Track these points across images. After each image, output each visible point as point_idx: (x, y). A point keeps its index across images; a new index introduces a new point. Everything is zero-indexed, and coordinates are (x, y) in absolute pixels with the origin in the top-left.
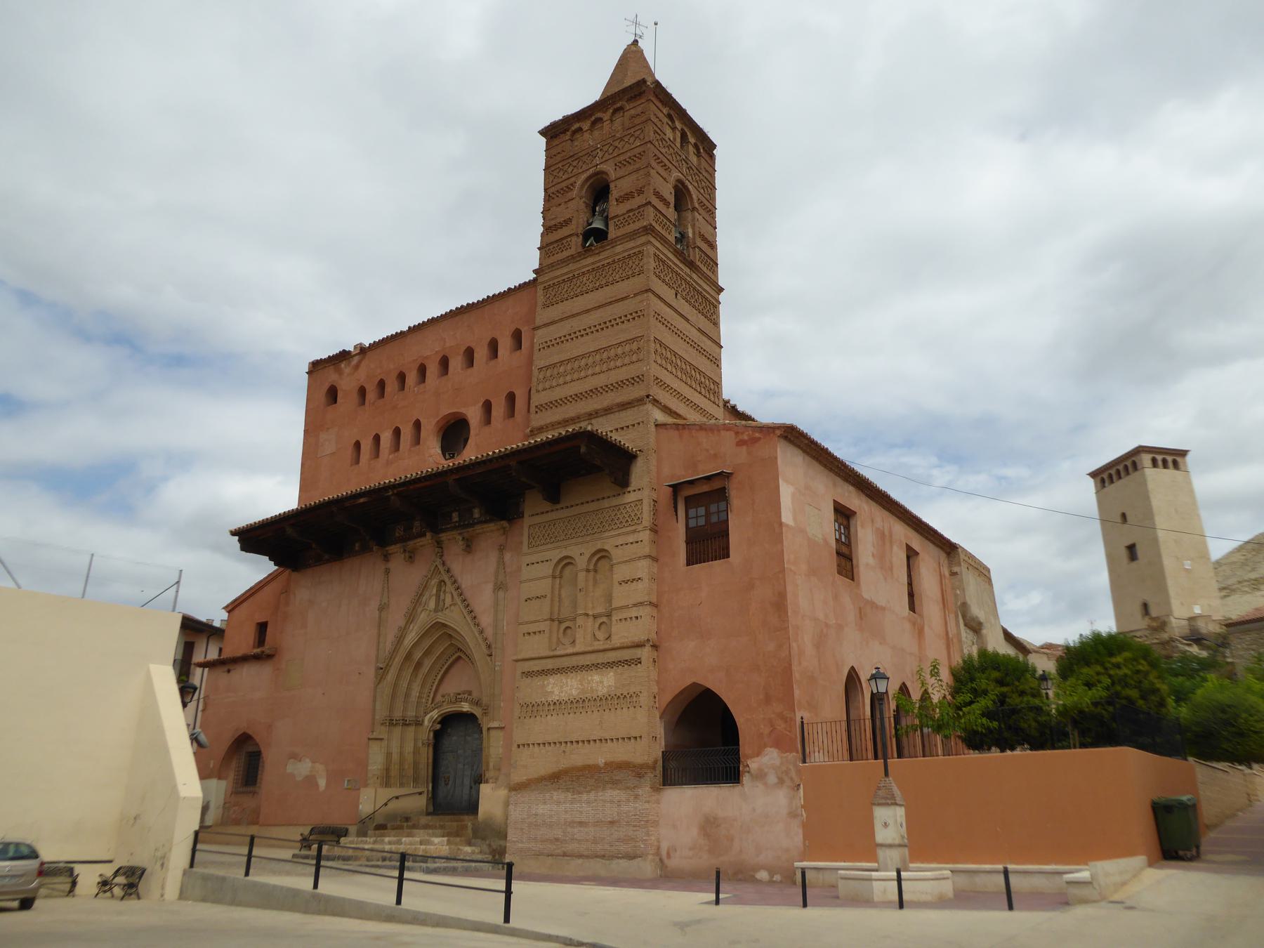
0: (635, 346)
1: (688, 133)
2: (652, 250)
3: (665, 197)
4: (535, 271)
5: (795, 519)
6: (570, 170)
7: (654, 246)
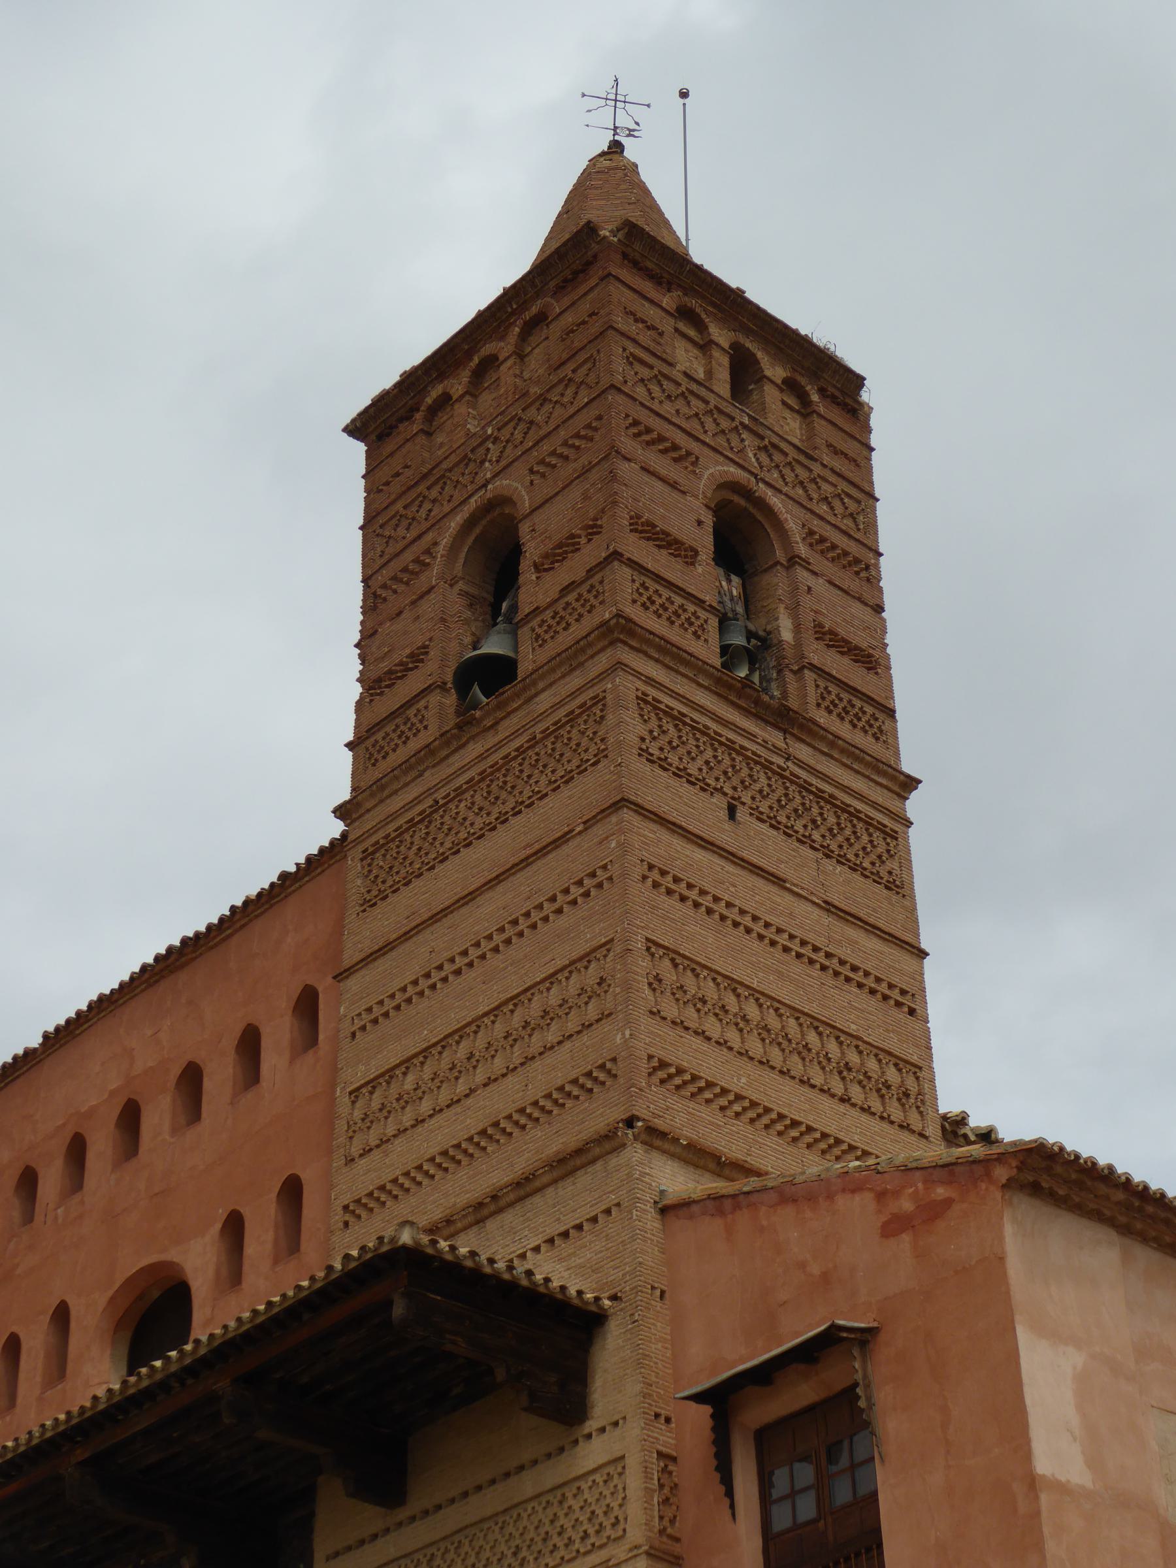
0: (591, 976)
1: (759, 355)
2: (628, 687)
3: (675, 532)
4: (341, 812)
5: (1094, 1462)
6: (423, 513)
7: (638, 674)
